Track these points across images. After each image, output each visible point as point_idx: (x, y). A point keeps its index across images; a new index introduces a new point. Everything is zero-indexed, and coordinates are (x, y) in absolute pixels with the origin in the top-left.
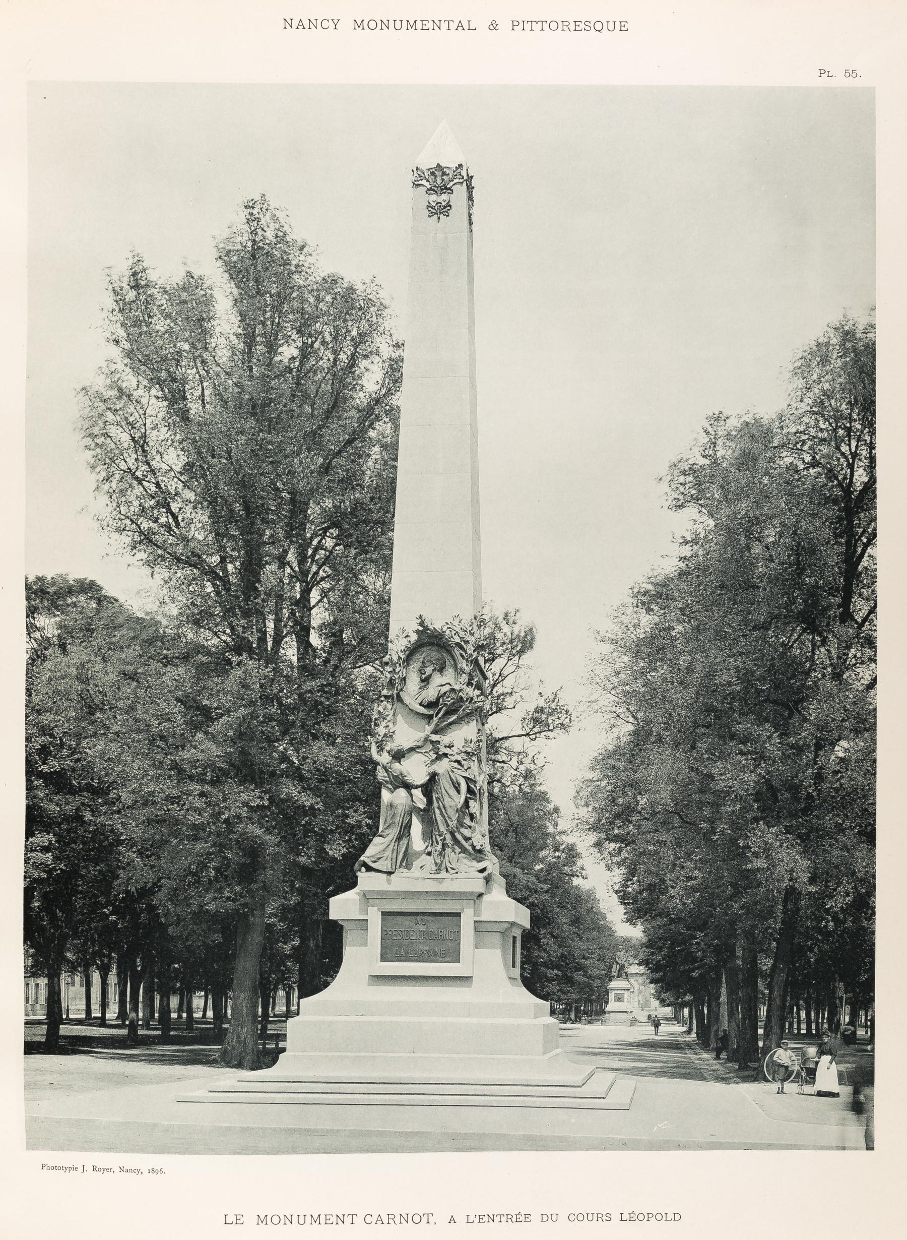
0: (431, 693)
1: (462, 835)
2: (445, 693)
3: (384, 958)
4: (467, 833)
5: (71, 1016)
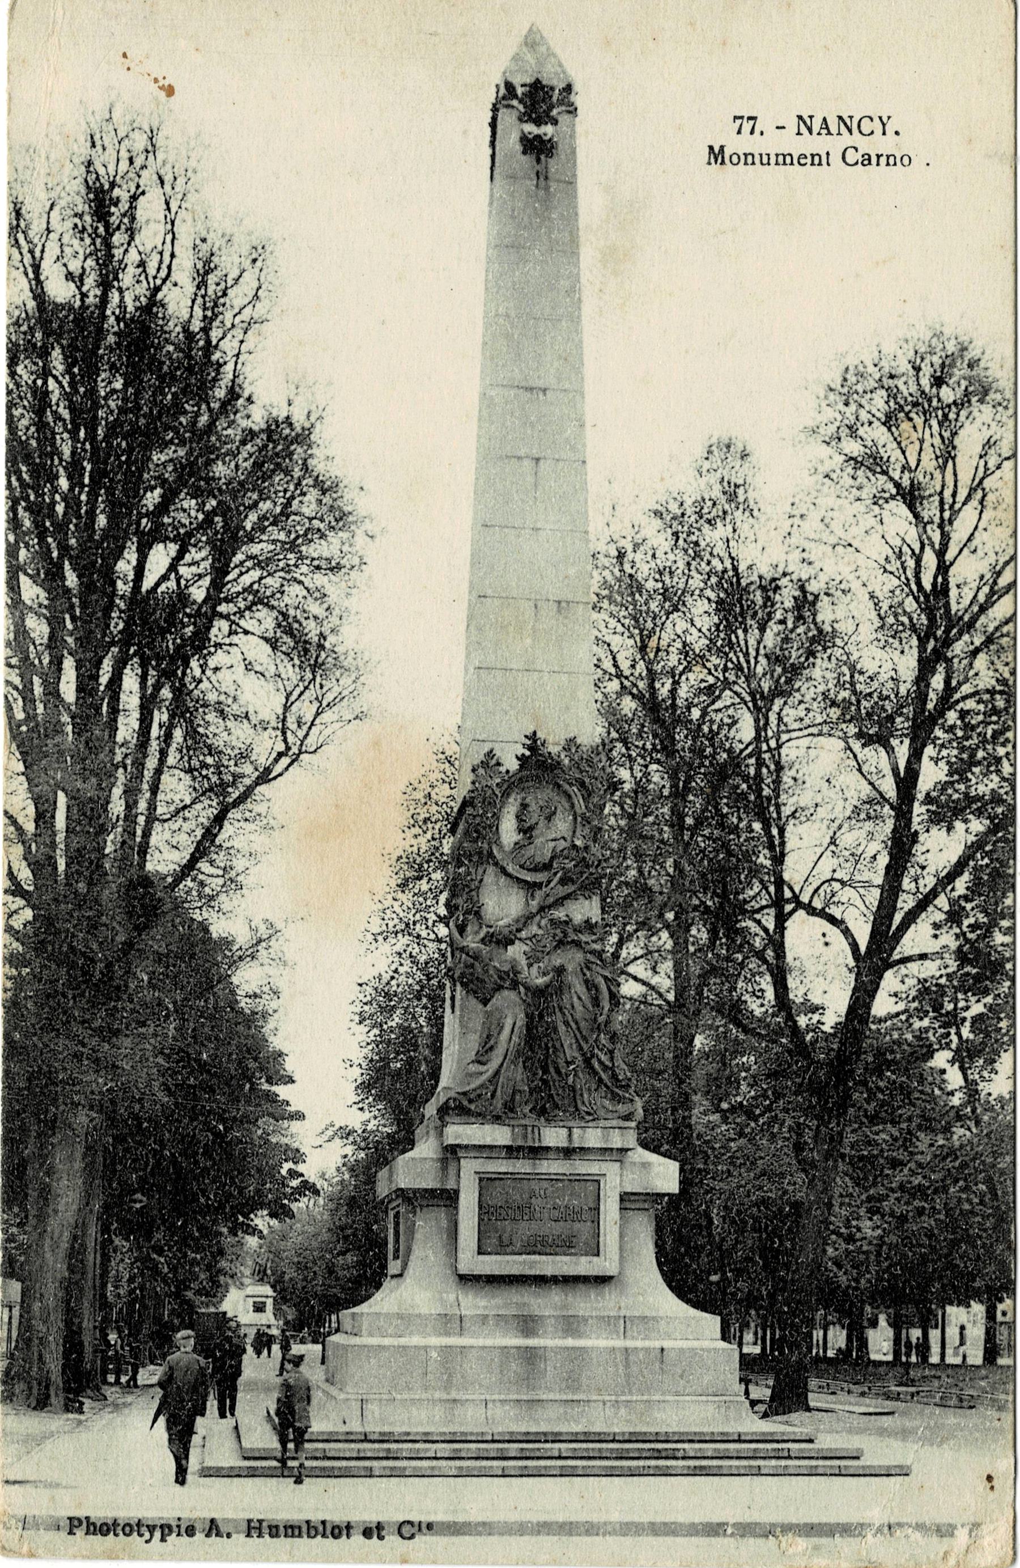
0: (543, 848)
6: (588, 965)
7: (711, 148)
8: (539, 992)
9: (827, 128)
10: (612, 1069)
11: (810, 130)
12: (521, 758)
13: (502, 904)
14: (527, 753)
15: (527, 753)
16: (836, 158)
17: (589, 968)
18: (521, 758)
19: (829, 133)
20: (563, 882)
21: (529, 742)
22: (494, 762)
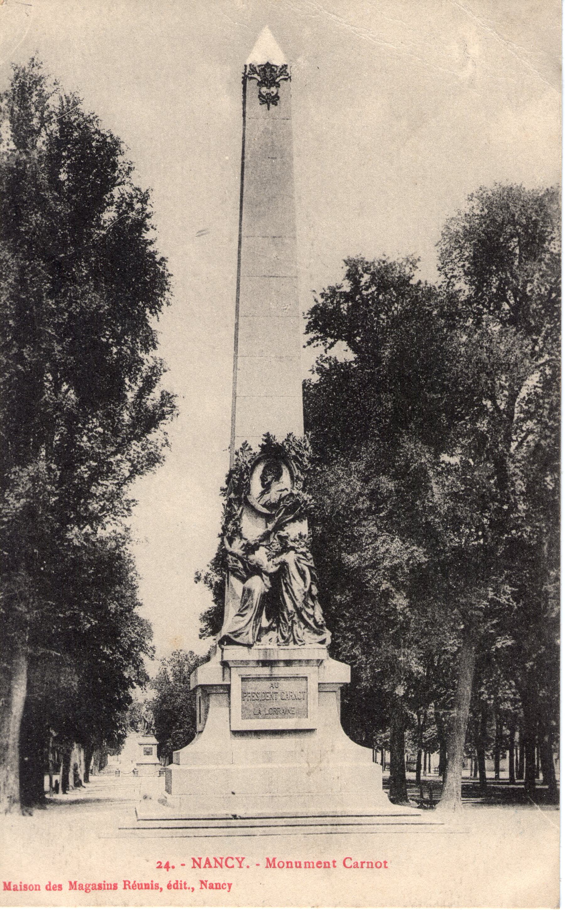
0: (273, 496)
1: (307, 613)
2: (285, 497)
3: (244, 717)
4: (310, 611)
5: (422, 778)
6: (299, 560)
7: (268, 859)
9: (209, 863)
11: (199, 866)
12: (262, 447)
13: (252, 528)
14: (265, 443)
15: (265, 443)
16: (339, 864)
17: (299, 562)
18: (262, 447)
19: (210, 867)
20: (286, 513)
21: (265, 438)
22: (247, 448)
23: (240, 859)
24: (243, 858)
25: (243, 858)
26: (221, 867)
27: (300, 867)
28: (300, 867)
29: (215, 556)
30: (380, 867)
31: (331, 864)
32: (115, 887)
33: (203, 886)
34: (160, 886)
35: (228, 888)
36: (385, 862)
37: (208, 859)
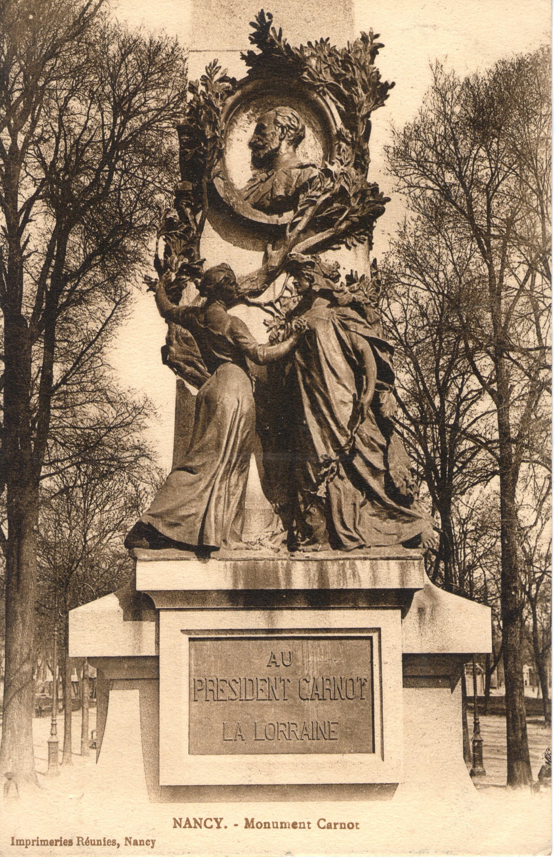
1: (368, 464)
8: (275, 364)
9: (189, 823)
10: (386, 473)
11: (180, 826)
12: (249, 58)
17: (346, 328)
19: (190, 827)
23: (219, 820)
24: (221, 819)
25: (221, 819)
26: (201, 827)
27: (269, 827)
28: (269, 827)
29: (163, 320)
30: (352, 828)
31: (306, 825)
32: (70, 843)
33: (128, 843)
34: (117, 842)
35: (151, 845)
36: (309, 823)
37: (188, 820)
